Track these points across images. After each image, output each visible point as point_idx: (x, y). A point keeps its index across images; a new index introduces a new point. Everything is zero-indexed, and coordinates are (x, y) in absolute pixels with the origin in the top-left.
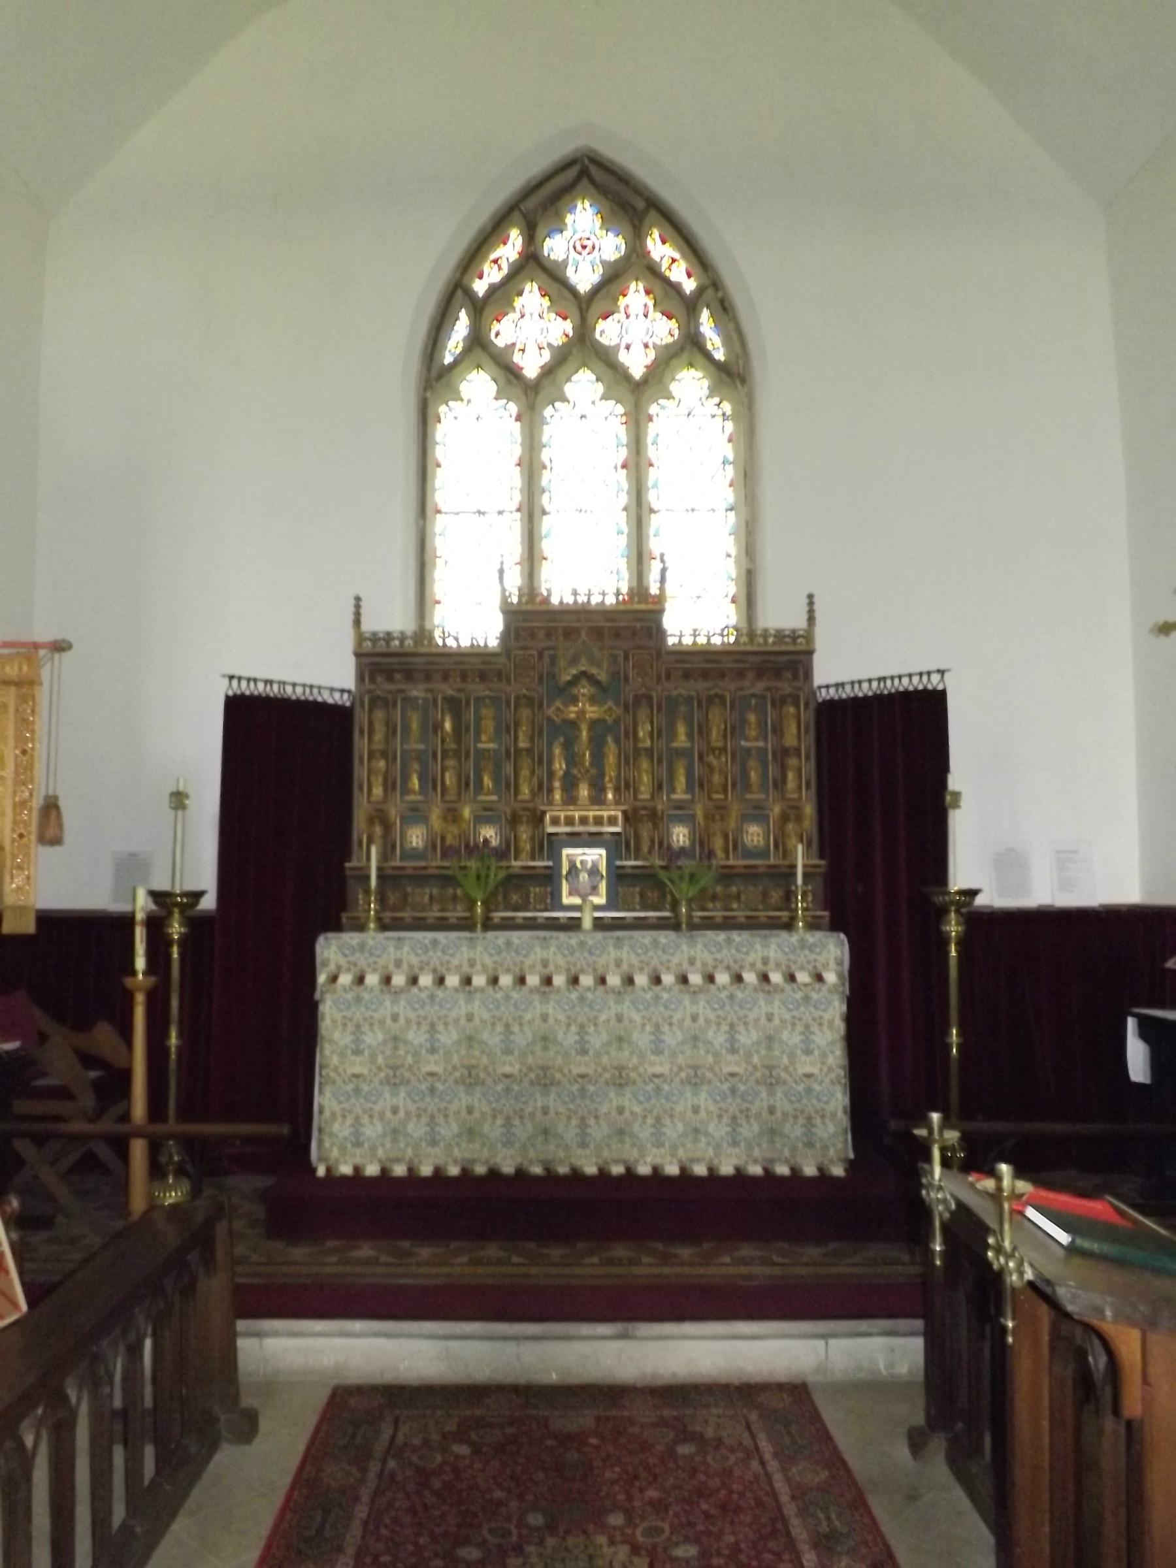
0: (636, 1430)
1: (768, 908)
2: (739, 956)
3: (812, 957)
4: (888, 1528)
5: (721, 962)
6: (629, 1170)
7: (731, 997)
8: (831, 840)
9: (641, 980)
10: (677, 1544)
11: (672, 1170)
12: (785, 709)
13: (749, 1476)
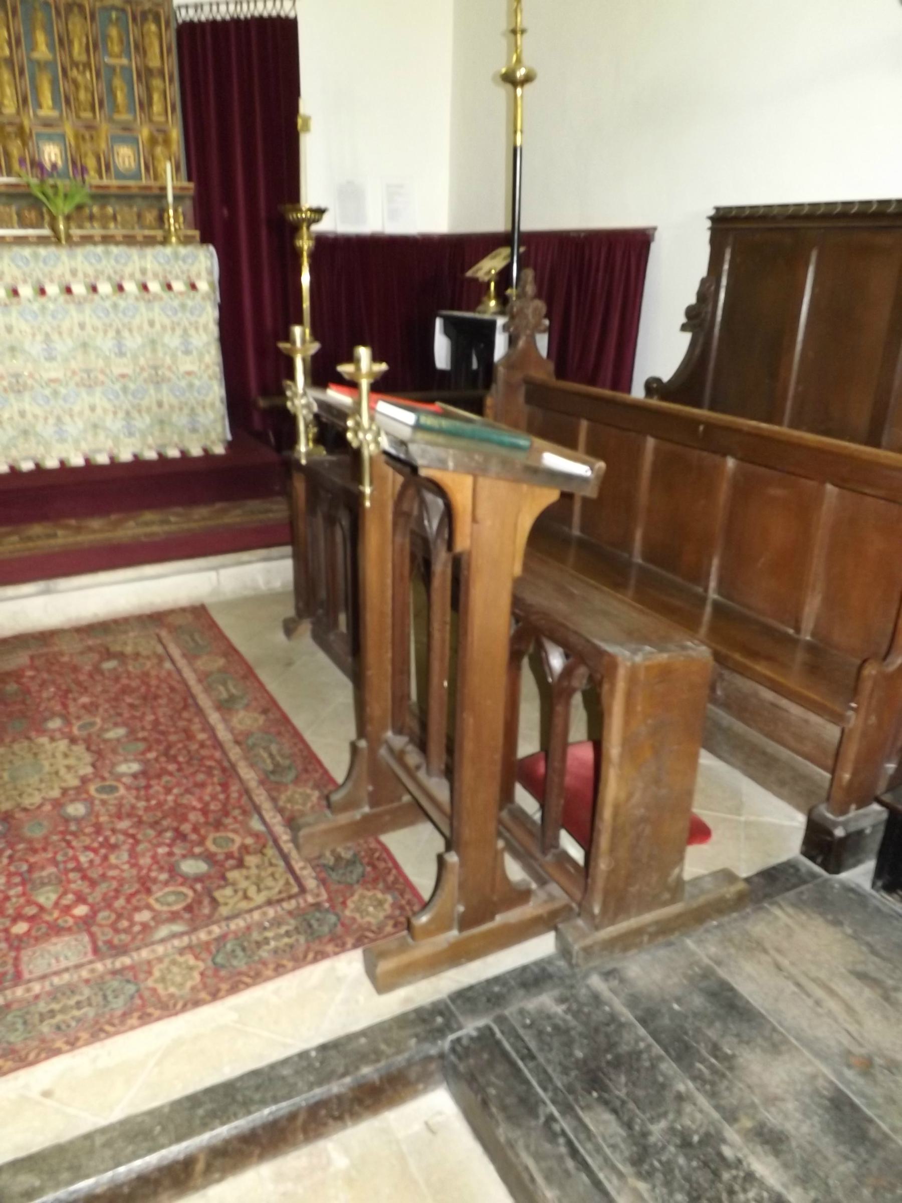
0: (65, 659)
1: (142, 227)
2: (118, 267)
3: (185, 267)
4: (273, 687)
5: (102, 272)
6: (37, 465)
7: (115, 306)
8: (197, 163)
9: (26, 291)
10: (107, 730)
11: (77, 461)
12: (146, 27)
13: (163, 674)
